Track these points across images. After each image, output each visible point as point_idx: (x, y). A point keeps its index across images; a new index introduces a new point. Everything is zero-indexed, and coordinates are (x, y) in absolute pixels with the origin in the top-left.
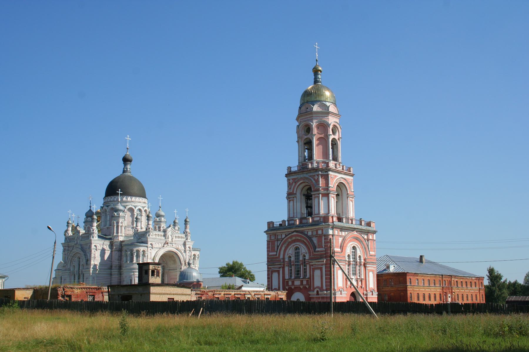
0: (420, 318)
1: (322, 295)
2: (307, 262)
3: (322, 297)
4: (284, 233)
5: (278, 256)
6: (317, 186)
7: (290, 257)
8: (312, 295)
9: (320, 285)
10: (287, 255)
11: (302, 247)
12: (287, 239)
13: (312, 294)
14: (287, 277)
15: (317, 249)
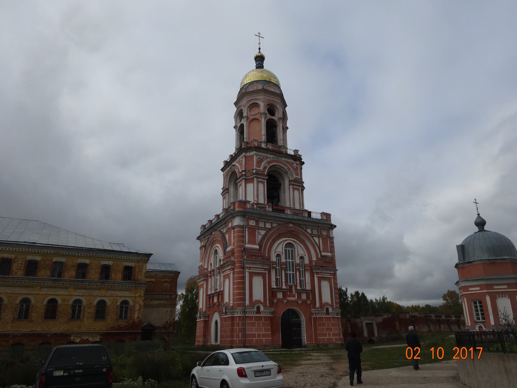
1: (252, 313)
9: (329, 301)
15: (323, 254)
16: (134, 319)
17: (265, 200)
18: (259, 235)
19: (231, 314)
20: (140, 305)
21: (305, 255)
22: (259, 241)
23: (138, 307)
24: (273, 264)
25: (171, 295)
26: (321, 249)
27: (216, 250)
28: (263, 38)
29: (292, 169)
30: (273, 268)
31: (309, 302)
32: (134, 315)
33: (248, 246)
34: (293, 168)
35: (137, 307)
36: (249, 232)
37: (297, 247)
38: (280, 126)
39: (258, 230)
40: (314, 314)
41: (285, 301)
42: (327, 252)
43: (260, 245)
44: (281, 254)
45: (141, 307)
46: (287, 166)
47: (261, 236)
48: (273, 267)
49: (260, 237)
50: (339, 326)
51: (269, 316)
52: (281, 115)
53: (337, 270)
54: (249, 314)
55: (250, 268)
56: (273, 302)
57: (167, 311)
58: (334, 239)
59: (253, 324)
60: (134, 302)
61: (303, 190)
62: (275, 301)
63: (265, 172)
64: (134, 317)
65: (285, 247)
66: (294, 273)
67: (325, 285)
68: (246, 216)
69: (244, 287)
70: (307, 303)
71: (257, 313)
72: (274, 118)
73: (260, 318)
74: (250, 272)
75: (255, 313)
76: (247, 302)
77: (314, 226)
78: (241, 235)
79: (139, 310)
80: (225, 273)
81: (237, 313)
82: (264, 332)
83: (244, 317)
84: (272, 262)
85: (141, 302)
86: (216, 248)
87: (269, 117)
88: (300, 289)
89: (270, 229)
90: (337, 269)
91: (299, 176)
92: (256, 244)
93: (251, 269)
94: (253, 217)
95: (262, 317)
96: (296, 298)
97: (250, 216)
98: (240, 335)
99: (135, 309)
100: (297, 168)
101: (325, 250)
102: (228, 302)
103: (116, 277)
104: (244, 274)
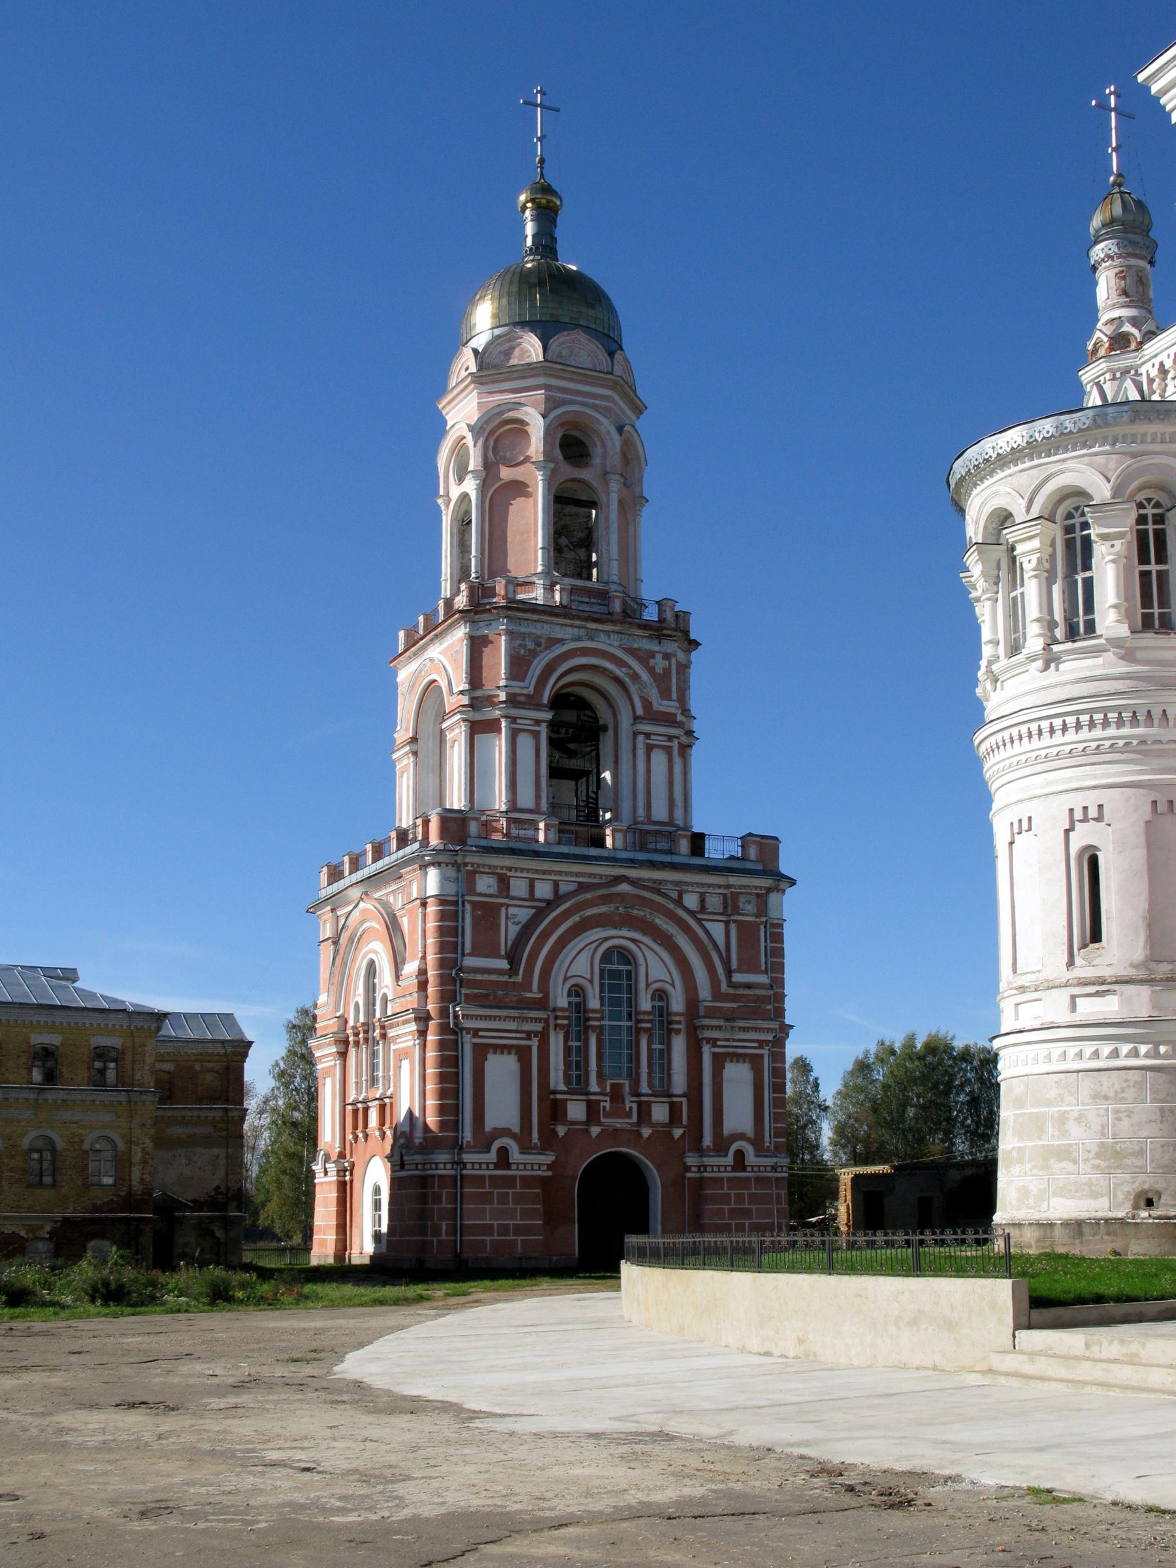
0: (417, 1481)
1: (476, 1166)
2: (648, 1025)
3: (757, 1179)
4: (525, 875)
5: (519, 979)
6: (486, 601)
7: (577, 991)
8: (716, 1169)
9: (747, 1127)
10: (566, 979)
11: (649, 954)
12: (694, 932)
13: (480, 1164)
14: (557, 1080)
15: (738, 978)
16: (130, 1186)
17: (538, 797)
18: (510, 924)
19: (417, 1169)
20: (143, 1149)
21: (673, 985)
22: (510, 943)
23: (140, 1154)
24: (556, 1018)
25: (226, 1110)
26: (734, 964)
27: (372, 964)
28: (558, 111)
29: (645, 676)
30: (555, 1029)
31: (678, 1133)
32: (130, 1176)
33: (470, 962)
34: (651, 670)
35: (137, 1156)
36: (473, 917)
37: (644, 956)
38: (608, 507)
39: (507, 909)
40: (693, 1169)
41: (595, 1131)
42: (756, 970)
43: (513, 957)
44: (587, 984)
45: (148, 1153)
46: (626, 665)
47: (518, 928)
48: (556, 1026)
49: (514, 930)
50: (779, 1202)
51: (539, 1176)
52: (615, 461)
53: (792, 1027)
54: (473, 1169)
55: (476, 1032)
56: (555, 1133)
57: (218, 1157)
58: (785, 924)
59: (486, 1198)
60: (130, 1142)
61: (685, 749)
62: (561, 1130)
63: (542, 696)
64: (130, 1180)
65: (601, 962)
66: (633, 1038)
67: (738, 1077)
68: (465, 864)
69: (458, 1088)
70: (672, 1137)
71: (497, 1166)
72: (585, 474)
73: (509, 1181)
74: (475, 1045)
75: (491, 1166)
76: (468, 1135)
77: (710, 885)
78: (448, 926)
79: (144, 1162)
80: (400, 1043)
81: (434, 1166)
82: (521, 1220)
83: (456, 1177)
84: (554, 1010)
85: (147, 1141)
86: (372, 956)
87: (568, 471)
88: (650, 1092)
89: (549, 903)
90: (787, 1022)
91: (674, 696)
92: (499, 957)
93: (481, 1033)
94: (490, 867)
95: (514, 1177)
96: (635, 1119)
97: (479, 865)
98: (444, 1228)
99: (133, 1160)
100: (667, 671)
101: (749, 965)
102: (408, 1132)
103: (73, 1076)
104: (457, 1051)
